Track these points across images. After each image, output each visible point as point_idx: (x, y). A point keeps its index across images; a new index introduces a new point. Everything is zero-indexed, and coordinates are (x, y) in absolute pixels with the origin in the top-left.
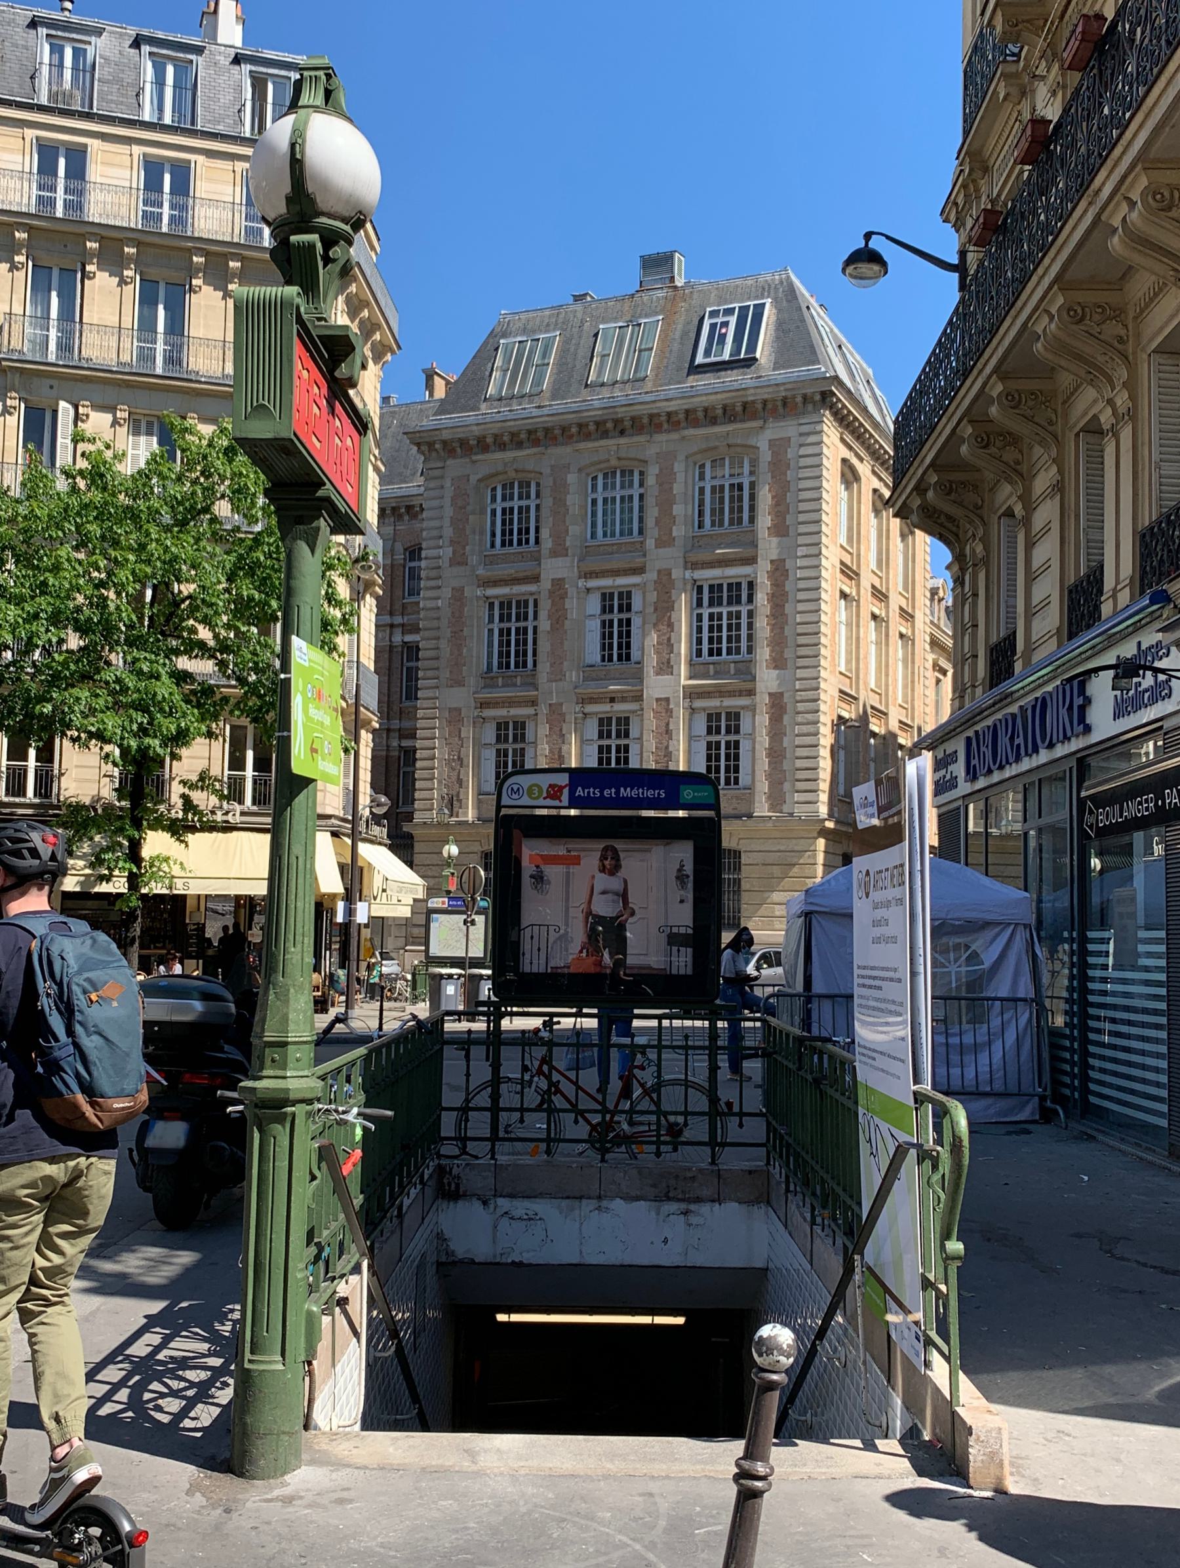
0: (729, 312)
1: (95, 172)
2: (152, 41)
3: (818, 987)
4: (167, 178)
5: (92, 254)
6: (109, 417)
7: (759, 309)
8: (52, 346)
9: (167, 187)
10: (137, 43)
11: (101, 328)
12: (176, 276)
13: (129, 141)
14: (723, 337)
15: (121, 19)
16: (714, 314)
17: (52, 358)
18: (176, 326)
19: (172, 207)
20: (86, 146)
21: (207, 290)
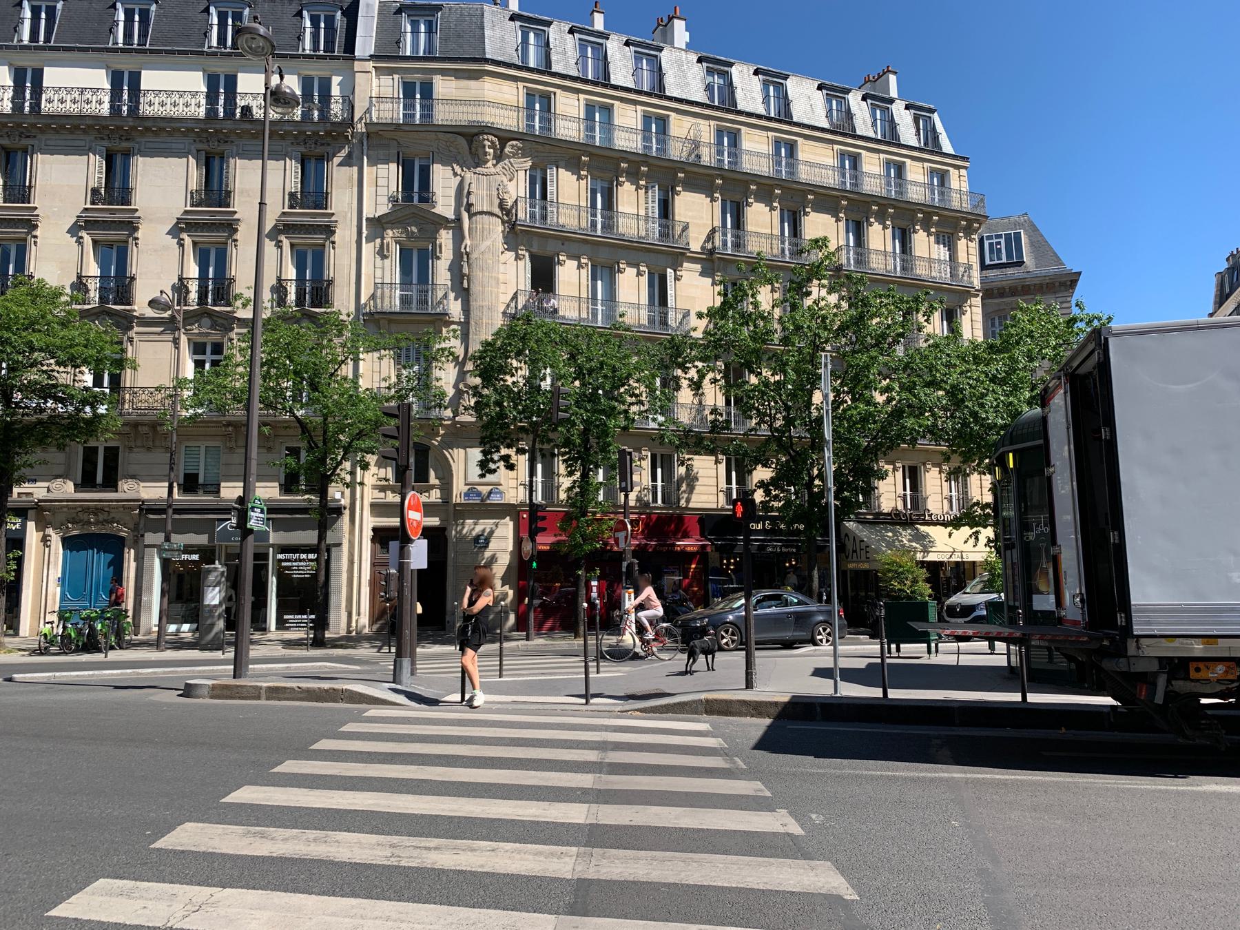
0: (999, 236)
1: (618, 120)
2: (764, 73)
3: (1143, 641)
4: (598, 113)
5: (623, 170)
6: (635, 270)
7: (1018, 236)
8: (599, 226)
9: (654, 130)
10: (571, 31)
11: (877, 252)
12: (737, 198)
13: (577, 91)
14: (999, 251)
15: (562, 18)
16: (989, 238)
17: (599, 233)
18: (609, 204)
19: (658, 143)
20: (668, 116)
21: (627, 184)
